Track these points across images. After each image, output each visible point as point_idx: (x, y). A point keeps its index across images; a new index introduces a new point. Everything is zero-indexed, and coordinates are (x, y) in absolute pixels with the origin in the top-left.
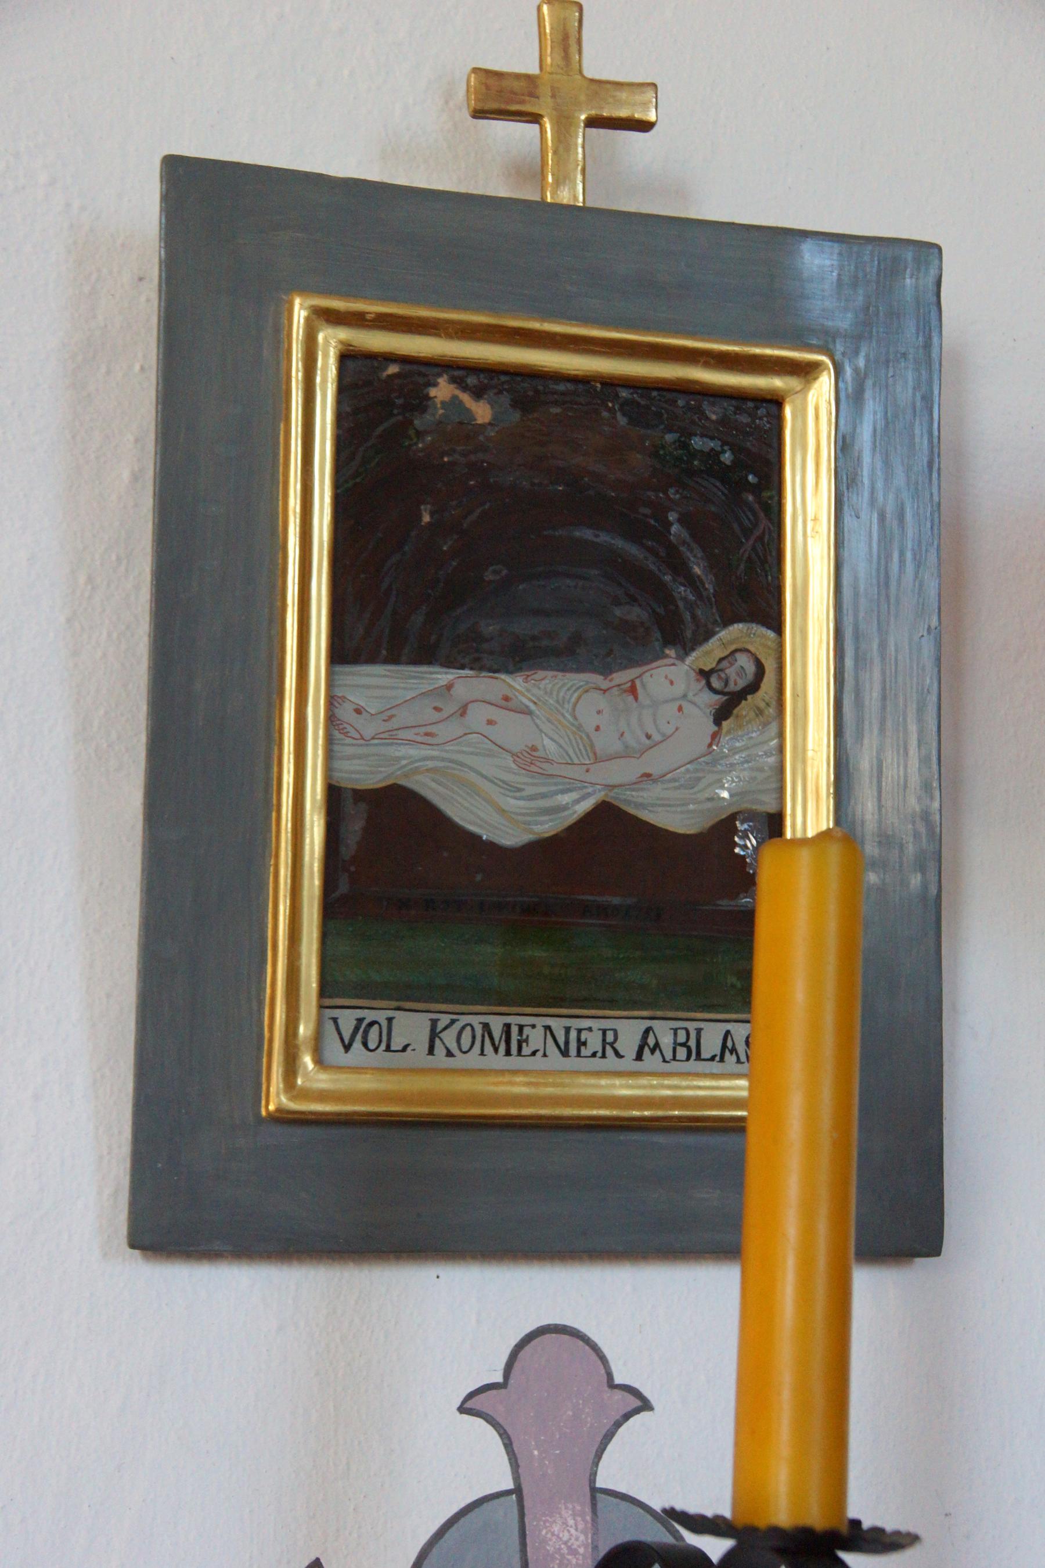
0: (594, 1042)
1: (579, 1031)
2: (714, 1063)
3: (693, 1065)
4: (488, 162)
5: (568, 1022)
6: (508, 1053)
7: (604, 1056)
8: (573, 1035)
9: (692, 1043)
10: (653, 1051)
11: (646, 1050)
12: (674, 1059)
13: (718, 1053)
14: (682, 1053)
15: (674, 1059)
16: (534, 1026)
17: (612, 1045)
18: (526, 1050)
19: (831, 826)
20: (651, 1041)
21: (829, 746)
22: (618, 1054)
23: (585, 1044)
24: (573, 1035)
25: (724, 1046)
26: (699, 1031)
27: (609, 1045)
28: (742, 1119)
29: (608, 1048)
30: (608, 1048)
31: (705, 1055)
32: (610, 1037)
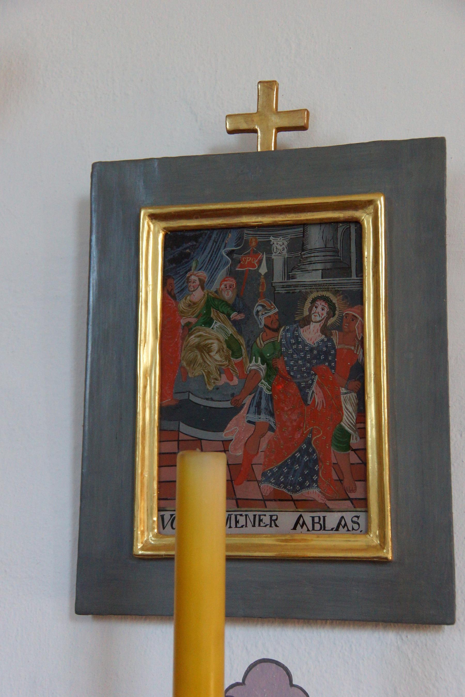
0: (266, 520)
1: (260, 516)
2: (321, 531)
3: (257, 529)
4: (233, 144)
5: (255, 513)
6: (254, 526)
7: (271, 526)
8: (257, 518)
9: (322, 522)
10: (344, 527)
11: (299, 526)
12: (313, 529)
13: (245, 524)
14: (317, 526)
15: (313, 529)
16: (265, 515)
17: (275, 521)
18: (262, 524)
19: (342, 423)
20: (343, 523)
21: (140, 356)
22: (276, 526)
23: (262, 520)
24: (257, 518)
25: (339, 524)
26: (324, 517)
27: (273, 522)
28: (173, 555)
29: (273, 522)
30: (273, 522)
31: (328, 526)
32: (274, 518)
